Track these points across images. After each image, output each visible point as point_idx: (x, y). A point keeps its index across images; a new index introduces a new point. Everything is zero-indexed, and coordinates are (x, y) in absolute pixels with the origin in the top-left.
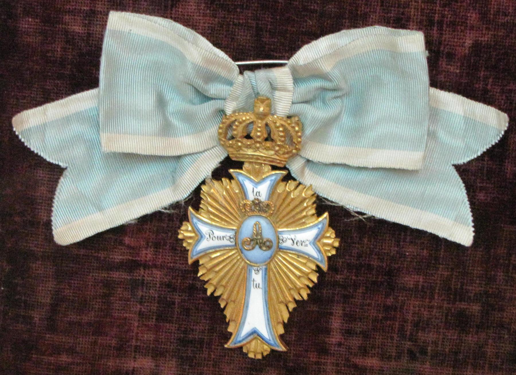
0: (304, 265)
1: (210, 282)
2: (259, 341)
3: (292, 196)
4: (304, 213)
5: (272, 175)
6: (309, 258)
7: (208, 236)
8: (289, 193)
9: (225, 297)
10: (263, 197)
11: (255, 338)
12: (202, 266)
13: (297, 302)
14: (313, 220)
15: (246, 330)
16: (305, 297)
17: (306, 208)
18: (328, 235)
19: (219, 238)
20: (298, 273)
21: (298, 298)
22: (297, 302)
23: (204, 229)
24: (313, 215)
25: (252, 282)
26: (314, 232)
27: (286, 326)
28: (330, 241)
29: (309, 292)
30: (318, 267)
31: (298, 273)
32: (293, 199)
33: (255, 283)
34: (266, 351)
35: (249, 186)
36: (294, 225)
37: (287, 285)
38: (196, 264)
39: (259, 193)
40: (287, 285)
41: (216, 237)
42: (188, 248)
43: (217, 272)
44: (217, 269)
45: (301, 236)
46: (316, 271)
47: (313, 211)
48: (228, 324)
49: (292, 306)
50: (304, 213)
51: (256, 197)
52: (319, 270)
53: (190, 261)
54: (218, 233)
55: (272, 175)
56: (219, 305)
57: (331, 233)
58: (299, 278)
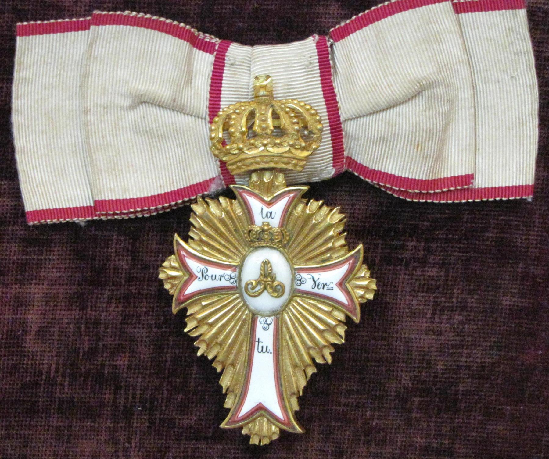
0: (329, 314)
1: (201, 338)
2: (265, 419)
3: (314, 221)
4: (330, 245)
5: (289, 192)
6: (334, 303)
7: (199, 275)
8: (310, 217)
9: (220, 358)
10: (275, 223)
11: (262, 416)
12: (190, 317)
13: (317, 365)
14: (342, 252)
15: (247, 407)
16: (329, 360)
17: (332, 237)
18: (363, 275)
19: (213, 278)
20: (321, 327)
21: (319, 361)
22: (317, 365)
23: (194, 266)
24: (343, 246)
25: (257, 343)
26: (343, 270)
27: (300, 399)
28: (365, 283)
29: (333, 351)
30: (348, 318)
31: (321, 327)
32: (315, 225)
33: (261, 345)
34: (274, 433)
35: (255, 204)
36: (313, 261)
37: (303, 342)
38: (183, 313)
39: (271, 213)
40: (303, 342)
41: (210, 275)
42: (171, 292)
43: (211, 325)
44: (211, 321)
45: (324, 277)
46: (346, 324)
47: (342, 242)
48: (224, 396)
49: (311, 371)
50: (330, 245)
51: (266, 220)
52: (348, 321)
53: (175, 309)
54: (213, 271)
55: (289, 192)
56: (215, 369)
57: (364, 272)
58: (320, 332)
